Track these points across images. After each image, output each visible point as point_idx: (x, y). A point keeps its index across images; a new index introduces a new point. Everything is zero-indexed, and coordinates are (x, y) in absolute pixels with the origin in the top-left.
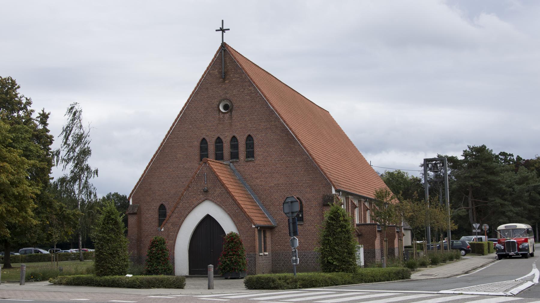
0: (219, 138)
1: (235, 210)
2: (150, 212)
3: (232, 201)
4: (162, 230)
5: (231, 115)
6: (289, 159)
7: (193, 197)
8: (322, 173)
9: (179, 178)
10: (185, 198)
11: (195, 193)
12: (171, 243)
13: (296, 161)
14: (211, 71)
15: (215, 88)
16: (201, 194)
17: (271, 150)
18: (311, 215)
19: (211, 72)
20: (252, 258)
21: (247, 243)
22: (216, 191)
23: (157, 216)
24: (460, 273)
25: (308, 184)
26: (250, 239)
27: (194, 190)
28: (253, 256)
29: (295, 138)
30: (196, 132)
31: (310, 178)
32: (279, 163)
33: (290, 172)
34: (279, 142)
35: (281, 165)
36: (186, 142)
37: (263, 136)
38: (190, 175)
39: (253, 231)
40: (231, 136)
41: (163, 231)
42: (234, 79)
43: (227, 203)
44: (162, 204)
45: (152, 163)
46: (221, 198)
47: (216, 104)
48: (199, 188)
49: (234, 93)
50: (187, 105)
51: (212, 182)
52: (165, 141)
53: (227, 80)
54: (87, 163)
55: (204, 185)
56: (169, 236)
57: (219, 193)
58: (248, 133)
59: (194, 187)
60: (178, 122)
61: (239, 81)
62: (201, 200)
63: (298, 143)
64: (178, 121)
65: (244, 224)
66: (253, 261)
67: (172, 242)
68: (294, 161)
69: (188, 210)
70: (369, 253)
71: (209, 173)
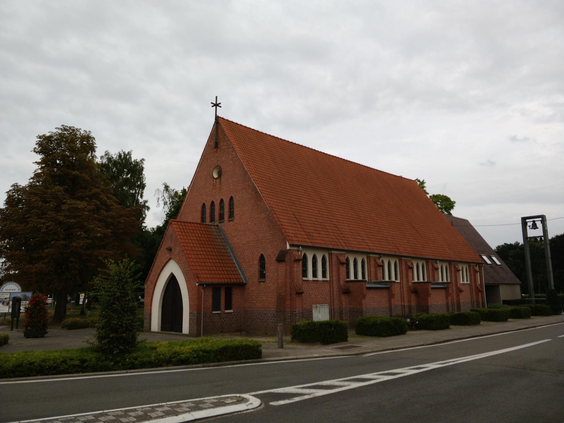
5: (220, 180)
6: (257, 216)
13: (261, 218)
18: (271, 271)
24: (450, 339)
42: (223, 147)
54: (150, 229)
70: (357, 312)
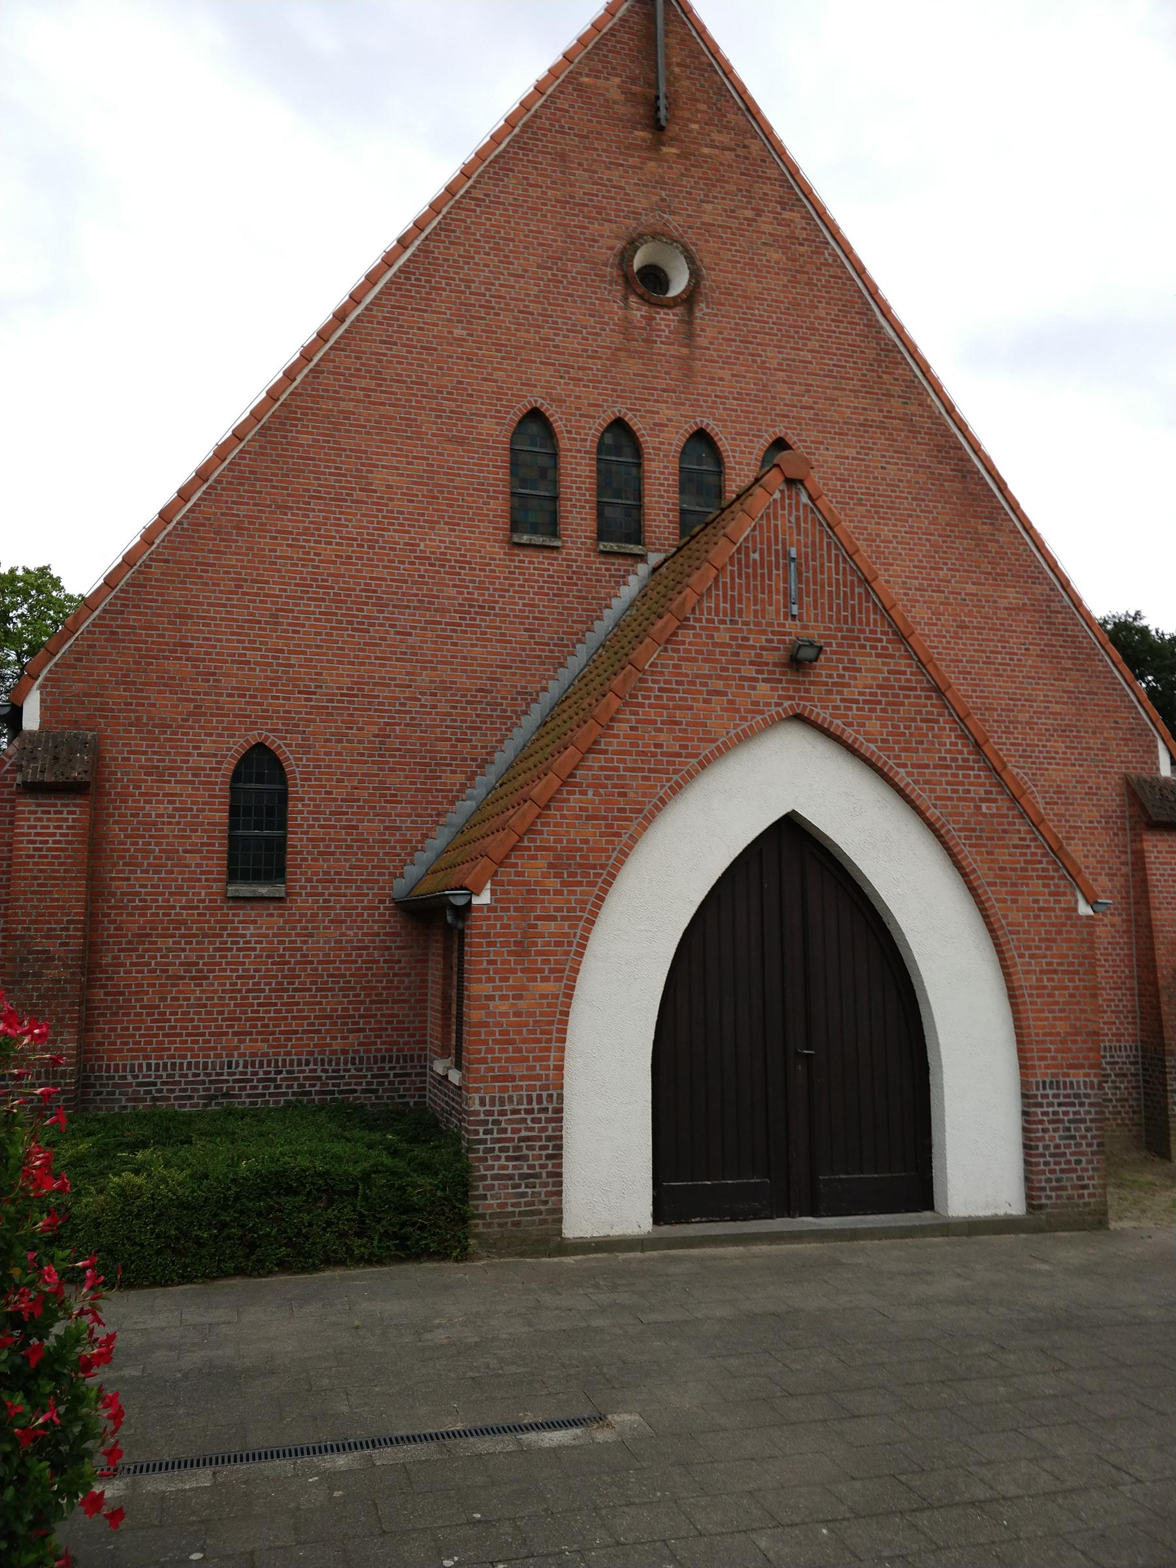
0: (619, 425)
1: (973, 800)
2: (168, 788)
3: (956, 744)
4: (476, 901)
7: (709, 693)
8: (1116, 678)
9: (381, 605)
10: (651, 689)
11: (724, 669)
12: (543, 996)
13: (1003, 603)
14: (587, 75)
15: (609, 169)
16: (764, 680)
17: (885, 531)
19: (586, 80)
20: (1082, 1104)
21: (1050, 1011)
22: (859, 670)
23: (222, 816)
25: (1056, 719)
26: (1066, 988)
27: (715, 645)
28: (1087, 1096)
29: (995, 496)
30: (495, 369)
31: (1064, 692)
32: (925, 602)
33: (975, 651)
34: (923, 500)
35: (933, 614)
36: (432, 410)
37: (847, 458)
38: (449, 598)
39: (1083, 941)
40: (690, 427)
41: (490, 908)
42: (706, 151)
43: (924, 751)
44: (260, 747)
45: (198, 494)
46: (892, 719)
47: (611, 248)
48: (746, 639)
49: (706, 219)
50: (445, 210)
51: (831, 609)
52: (299, 378)
53: (672, 146)
55: (779, 625)
56: (535, 944)
57: (879, 687)
58: (777, 430)
59: (718, 629)
60: (381, 292)
61: (730, 166)
62: (759, 718)
63: (1011, 520)
64: (386, 286)
65: (1029, 894)
66: (1088, 1129)
67: (551, 987)
68: (995, 602)
69: (676, 772)
71: (813, 553)
